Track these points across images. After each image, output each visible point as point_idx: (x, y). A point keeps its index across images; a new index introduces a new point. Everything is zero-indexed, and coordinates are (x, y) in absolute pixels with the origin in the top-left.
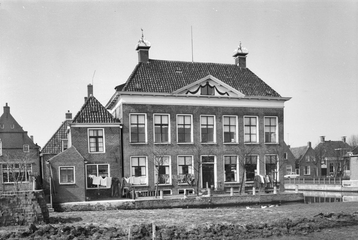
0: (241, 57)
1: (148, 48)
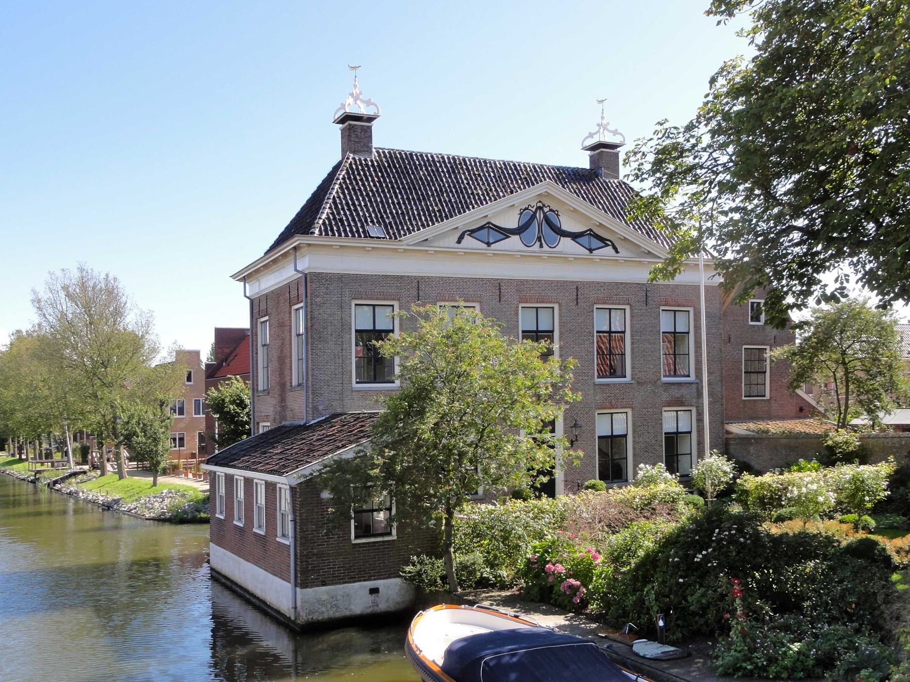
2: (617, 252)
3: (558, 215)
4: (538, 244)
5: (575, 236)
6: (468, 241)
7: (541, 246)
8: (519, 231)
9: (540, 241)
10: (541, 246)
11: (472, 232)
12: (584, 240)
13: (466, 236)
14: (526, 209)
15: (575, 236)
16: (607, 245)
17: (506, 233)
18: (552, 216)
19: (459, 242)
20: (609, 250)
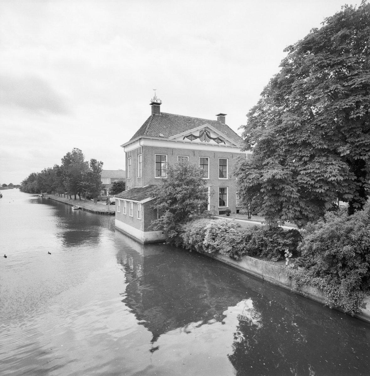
2: (225, 144)
3: (210, 133)
4: (204, 141)
5: (214, 139)
6: (186, 140)
7: (205, 141)
8: (199, 137)
11: (187, 137)
12: (216, 140)
13: (186, 138)
14: (202, 131)
15: (214, 139)
18: (208, 133)
19: (184, 139)
20: (223, 144)
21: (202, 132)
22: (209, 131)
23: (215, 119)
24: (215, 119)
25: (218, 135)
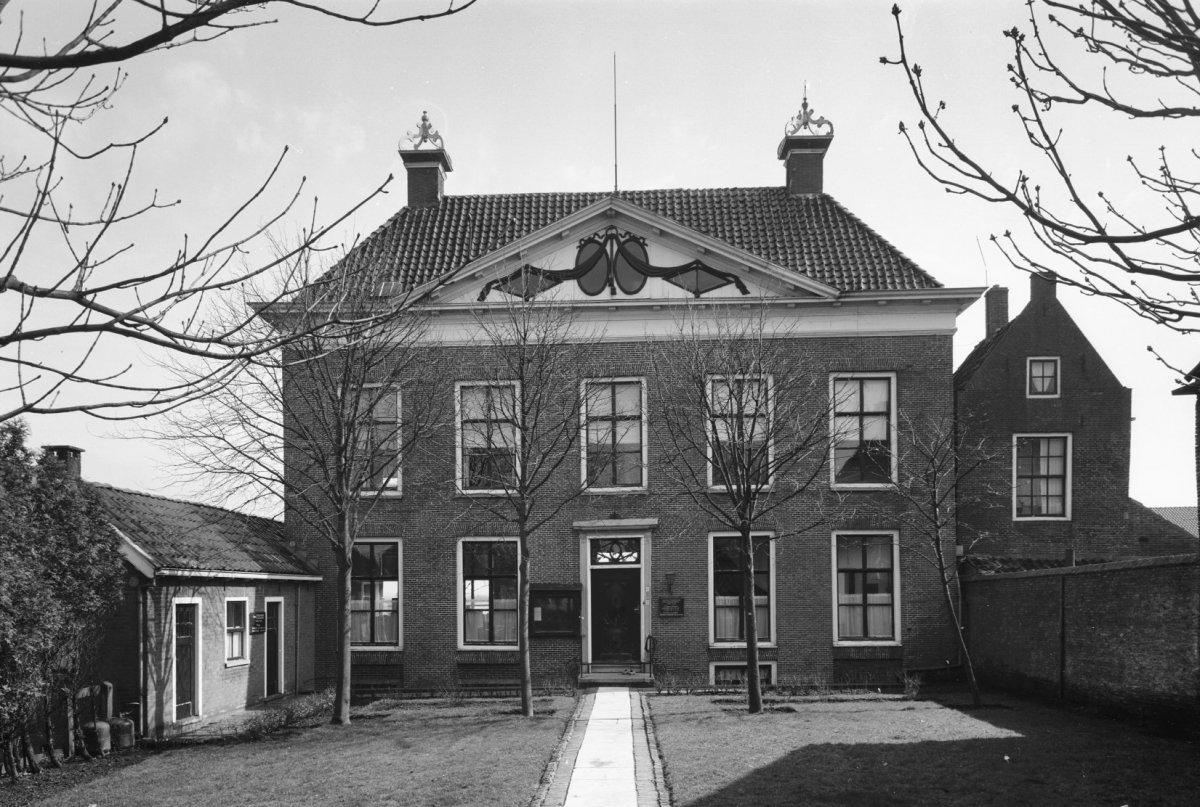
0: (804, 154)
1: (824, 143)
2: (744, 291)
3: (643, 246)
4: (607, 290)
6: (495, 297)
7: (613, 292)
9: (611, 285)
10: (613, 292)
15: (668, 274)
16: (729, 282)
17: (556, 277)
18: (631, 248)
19: (482, 297)
20: (730, 291)
21: (592, 249)
22: (637, 232)
23: (775, 176)
24: (775, 176)
25: (473, 278)
